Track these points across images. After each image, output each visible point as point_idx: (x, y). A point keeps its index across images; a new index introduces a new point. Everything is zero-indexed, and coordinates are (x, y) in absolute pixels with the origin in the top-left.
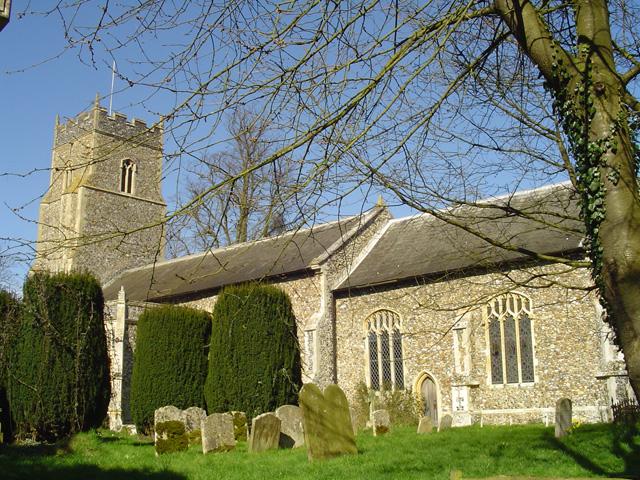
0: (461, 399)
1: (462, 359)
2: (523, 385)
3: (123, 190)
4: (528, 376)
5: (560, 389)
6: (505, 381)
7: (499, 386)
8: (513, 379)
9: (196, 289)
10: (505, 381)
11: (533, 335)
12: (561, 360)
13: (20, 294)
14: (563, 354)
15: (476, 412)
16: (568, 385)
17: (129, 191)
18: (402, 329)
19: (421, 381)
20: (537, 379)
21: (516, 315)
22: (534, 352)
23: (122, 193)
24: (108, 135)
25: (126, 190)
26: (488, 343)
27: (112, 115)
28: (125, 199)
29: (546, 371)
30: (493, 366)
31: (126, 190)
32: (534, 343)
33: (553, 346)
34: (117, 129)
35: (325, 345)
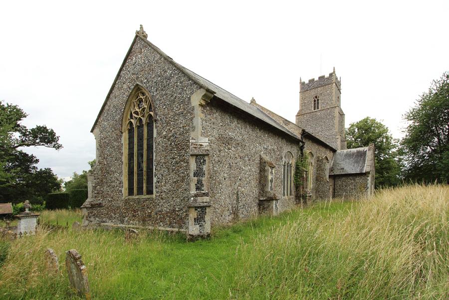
8: (140, 192)
25: (289, 195)
31: (289, 195)
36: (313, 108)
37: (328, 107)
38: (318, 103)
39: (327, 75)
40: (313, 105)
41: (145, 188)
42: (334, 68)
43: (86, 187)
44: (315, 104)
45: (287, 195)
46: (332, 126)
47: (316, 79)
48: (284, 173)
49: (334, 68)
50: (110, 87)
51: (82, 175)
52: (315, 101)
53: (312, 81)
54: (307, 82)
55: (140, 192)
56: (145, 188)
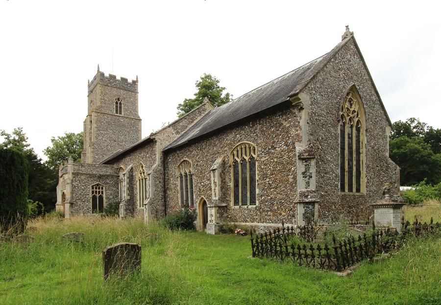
0: (212, 215)
1: (215, 189)
2: (250, 207)
3: (117, 113)
4: (253, 202)
5: (271, 211)
6: (240, 204)
7: (237, 207)
8: (244, 203)
9: (138, 152)
10: (240, 204)
11: (257, 172)
12: (272, 190)
13: (44, 158)
14: (274, 185)
15: (221, 224)
16: (276, 208)
17: (120, 113)
18: (193, 171)
19: (201, 205)
20: (257, 202)
21: (247, 158)
22: (257, 184)
23: (116, 114)
24: (106, 85)
25: (354, 190)
26: (232, 179)
27: (434, 222)
28: (118, 118)
29: (263, 198)
30: (235, 194)
31: (354, 190)
32: (257, 178)
33: (268, 180)
34: (110, 83)
35: (158, 182)
36: (115, 112)
37: (132, 117)
38: (120, 107)
39: (130, 81)
40: (115, 107)
41: (240, 200)
42: (137, 76)
43: (126, 210)
44: (117, 107)
45: (350, 190)
46: (136, 139)
47: (118, 78)
48: (192, 188)
49: (137, 76)
50: (365, 61)
51: (31, 157)
52: (117, 103)
53: (112, 77)
54: (107, 75)
55: (350, 190)
56: (240, 200)
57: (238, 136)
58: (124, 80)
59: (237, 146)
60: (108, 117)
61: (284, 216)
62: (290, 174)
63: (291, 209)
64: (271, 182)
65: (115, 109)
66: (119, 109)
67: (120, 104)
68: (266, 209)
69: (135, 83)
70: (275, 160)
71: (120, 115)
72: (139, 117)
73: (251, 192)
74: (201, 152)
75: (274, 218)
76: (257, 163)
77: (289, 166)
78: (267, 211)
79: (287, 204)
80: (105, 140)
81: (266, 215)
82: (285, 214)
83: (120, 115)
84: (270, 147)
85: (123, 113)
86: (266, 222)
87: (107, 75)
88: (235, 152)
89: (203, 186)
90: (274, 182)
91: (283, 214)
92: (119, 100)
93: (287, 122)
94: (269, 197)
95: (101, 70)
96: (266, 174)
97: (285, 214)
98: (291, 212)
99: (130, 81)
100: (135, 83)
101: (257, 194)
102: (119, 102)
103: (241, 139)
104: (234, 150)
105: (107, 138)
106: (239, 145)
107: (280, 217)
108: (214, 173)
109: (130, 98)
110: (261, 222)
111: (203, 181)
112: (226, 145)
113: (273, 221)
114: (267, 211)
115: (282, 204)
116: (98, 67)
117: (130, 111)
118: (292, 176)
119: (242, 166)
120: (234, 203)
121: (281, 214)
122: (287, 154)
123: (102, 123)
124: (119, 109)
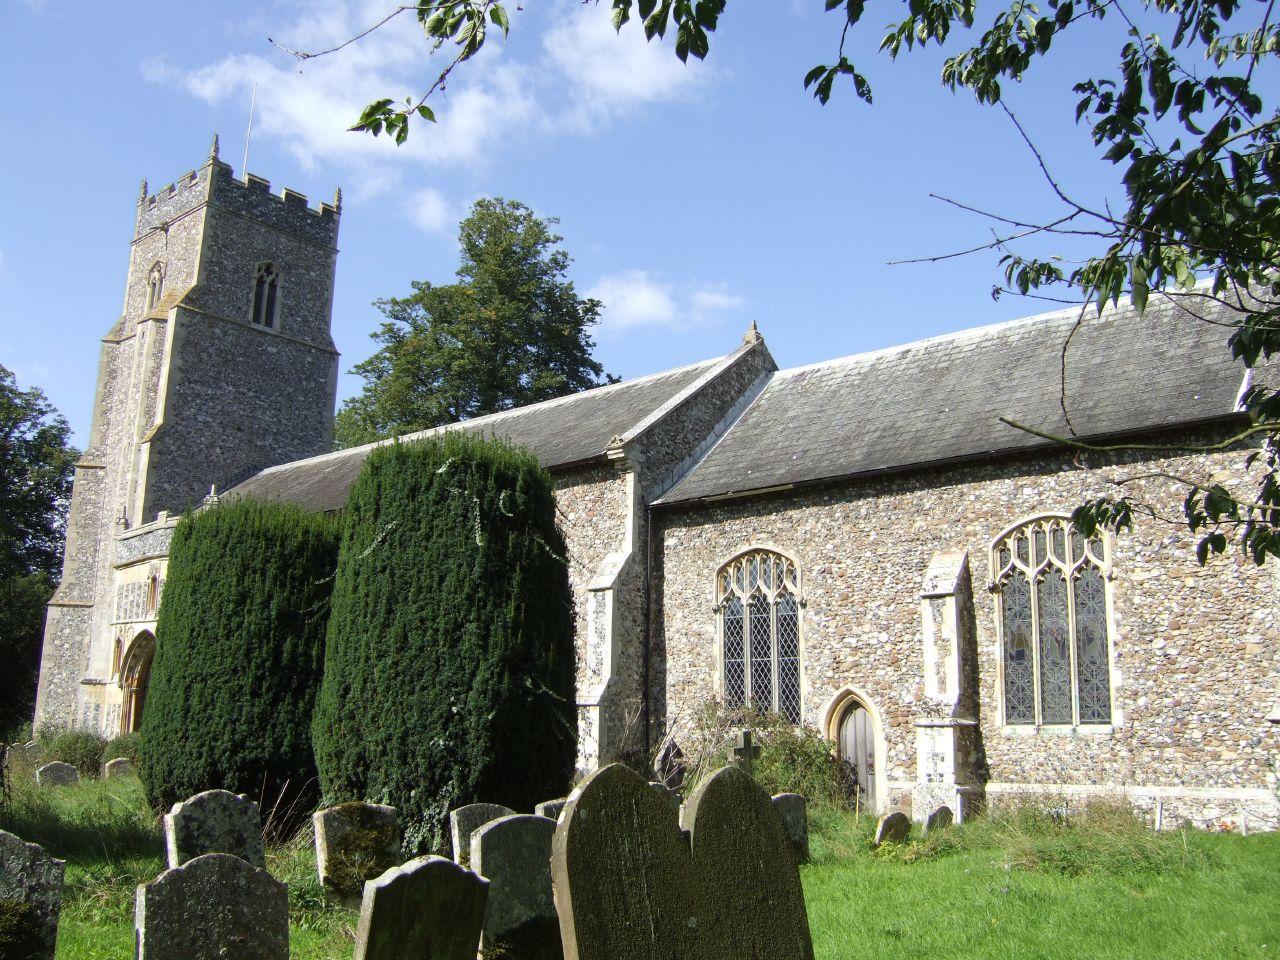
1: (939, 665)
2: (1085, 730)
3: (257, 319)
5: (1177, 744)
6: (1039, 719)
10: (1039, 719)
11: (1111, 616)
12: (1179, 676)
16: (1197, 735)
17: (269, 323)
20: (1118, 717)
26: (999, 630)
32: (1113, 634)
36: (250, 316)
40: (252, 296)
44: (259, 295)
49: (339, 189)
52: (261, 282)
53: (259, 187)
54: (242, 177)
57: (1028, 491)
58: (296, 201)
59: (1026, 524)
60: (225, 333)
61: (1230, 762)
62: (1250, 630)
63: (1259, 741)
64: (1173, 652)
65: (252, 304)
66: (264, 309)
67: (273, 286)
68: (1154, 738)
69: (330, 215)
70: (1190, 582)
71: (268, 330)
72: (331, 343)
73: (1083, 682)
74: (846, 528)
75: (1193, 769)
76: (1110, 589)
77: (1242, 607)
78: (1161, 746)
79: (1241, 723)
80: (206, 423)
81: (1154, 759)
82: (1233, 755)
83: (268, 330)
84: (1166, 541)
85: (277, 322)
86: (1156, 782)
87: (242, 177)
88: (1011, 543)
89: (857, 649)
90: (1188, 649)
91: (1227, 755)
92: (268, 271)
93: (1227, 472)
94: (1167, 701)
95: (222, 158)
96: (1154, 624)
97: (1233, 755)
98: (1257, 750)
99: (315, 205)
100: (330, 215)
101: (1117, 690)
102: (268, 280)
103: (1041, 503)
104: (1008, 535)
105: (214, 416)
106: (1031, 522)
107: (1213, 766)
108: (750, 562)
109: (309, 268)
110: (1135, 783)
111: (856, 630)
112: (972, 516)
113: (1185, 778)
114: (1161, 746)
115: (1222, 724)
116: (217, 142)
117: (305, 320)
118: (1257, 638)
119: (1039, 591)
120: (1008, 716)
121: (1216, 757)
122: (1235, 567)
123: (204, 356)
124: (264, 309)
